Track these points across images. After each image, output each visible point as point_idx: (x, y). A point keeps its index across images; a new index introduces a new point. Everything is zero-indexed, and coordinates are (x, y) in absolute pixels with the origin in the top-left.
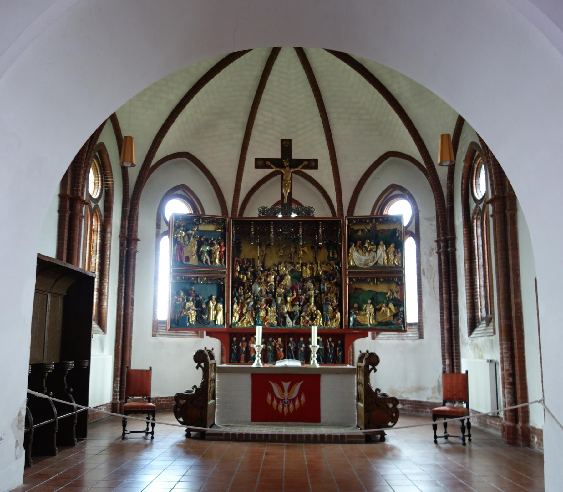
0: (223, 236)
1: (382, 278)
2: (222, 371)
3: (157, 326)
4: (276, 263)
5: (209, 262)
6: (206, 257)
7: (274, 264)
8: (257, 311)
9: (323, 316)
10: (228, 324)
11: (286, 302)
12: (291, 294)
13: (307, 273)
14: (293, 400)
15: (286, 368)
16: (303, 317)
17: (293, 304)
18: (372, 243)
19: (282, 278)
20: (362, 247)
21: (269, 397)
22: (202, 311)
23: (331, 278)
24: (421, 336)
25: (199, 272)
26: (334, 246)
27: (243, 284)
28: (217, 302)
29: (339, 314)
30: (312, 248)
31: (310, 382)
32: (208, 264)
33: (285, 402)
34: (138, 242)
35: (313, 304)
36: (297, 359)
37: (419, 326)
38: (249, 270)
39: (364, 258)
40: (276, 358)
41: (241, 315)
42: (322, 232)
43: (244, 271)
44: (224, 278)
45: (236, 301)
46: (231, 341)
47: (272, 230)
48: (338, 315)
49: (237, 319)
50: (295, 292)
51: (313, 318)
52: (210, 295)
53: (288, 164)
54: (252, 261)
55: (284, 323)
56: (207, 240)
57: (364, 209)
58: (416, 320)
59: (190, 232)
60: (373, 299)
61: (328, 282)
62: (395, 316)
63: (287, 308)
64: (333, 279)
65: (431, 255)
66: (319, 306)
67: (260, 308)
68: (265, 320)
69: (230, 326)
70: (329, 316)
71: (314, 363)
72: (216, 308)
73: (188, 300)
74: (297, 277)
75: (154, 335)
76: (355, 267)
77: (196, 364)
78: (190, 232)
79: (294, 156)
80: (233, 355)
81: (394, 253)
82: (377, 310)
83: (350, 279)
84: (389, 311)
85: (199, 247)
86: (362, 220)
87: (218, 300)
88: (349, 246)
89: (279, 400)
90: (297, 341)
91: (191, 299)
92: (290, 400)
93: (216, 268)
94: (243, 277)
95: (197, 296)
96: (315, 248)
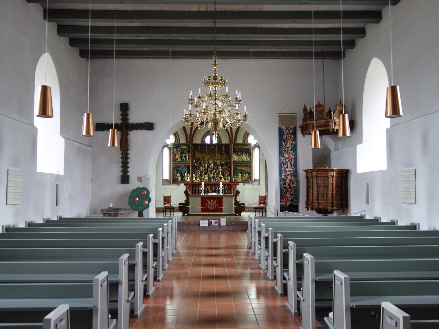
0: (189, 150)
2: (191, 196)
3: (164, 180)
6: (183, 158)
8: (201, 176)
9: (224, 178)
11: (211, 173)
13: (219, 163)
14: (214, 205)
15: (212, 195)
17: (214, 174)
19: (210, 165)
20: (237, 154)
21: (207, 205)
22: (183, 177)
24: (259, 184)
26: (228, 153)
27: (196, 167)
30: (220, 154)
31: (219, 200)
36: (215, 192)
37: (259, 180)
39: (238, 158)
40: (208, 193)
41: (196, 178)
43: (196, 162)
46: (193, 187)
51: (221, 179)
55: (211, 181)
56: (184, 152)
57: (240, 141)
58: (258, 179)
60: (241, 172)
62: (248, 178)
63: (212, 175)
66: (223, 175)
68: (204, 179)
69: (192, 182)
70: (226, 178)
71: (221, 194)
72: (187, 176)
74: (215, 164)
75: (163, 185)
76: (235, 161)
82: (242, 176)
83: (234, 165)
84: (246, 176)
85: (181, 154)
86: (238, 145)
87: (188, 173)
88: (233, 154)
90: (215, 187)
95: (181, 172)
96: (221, 153)
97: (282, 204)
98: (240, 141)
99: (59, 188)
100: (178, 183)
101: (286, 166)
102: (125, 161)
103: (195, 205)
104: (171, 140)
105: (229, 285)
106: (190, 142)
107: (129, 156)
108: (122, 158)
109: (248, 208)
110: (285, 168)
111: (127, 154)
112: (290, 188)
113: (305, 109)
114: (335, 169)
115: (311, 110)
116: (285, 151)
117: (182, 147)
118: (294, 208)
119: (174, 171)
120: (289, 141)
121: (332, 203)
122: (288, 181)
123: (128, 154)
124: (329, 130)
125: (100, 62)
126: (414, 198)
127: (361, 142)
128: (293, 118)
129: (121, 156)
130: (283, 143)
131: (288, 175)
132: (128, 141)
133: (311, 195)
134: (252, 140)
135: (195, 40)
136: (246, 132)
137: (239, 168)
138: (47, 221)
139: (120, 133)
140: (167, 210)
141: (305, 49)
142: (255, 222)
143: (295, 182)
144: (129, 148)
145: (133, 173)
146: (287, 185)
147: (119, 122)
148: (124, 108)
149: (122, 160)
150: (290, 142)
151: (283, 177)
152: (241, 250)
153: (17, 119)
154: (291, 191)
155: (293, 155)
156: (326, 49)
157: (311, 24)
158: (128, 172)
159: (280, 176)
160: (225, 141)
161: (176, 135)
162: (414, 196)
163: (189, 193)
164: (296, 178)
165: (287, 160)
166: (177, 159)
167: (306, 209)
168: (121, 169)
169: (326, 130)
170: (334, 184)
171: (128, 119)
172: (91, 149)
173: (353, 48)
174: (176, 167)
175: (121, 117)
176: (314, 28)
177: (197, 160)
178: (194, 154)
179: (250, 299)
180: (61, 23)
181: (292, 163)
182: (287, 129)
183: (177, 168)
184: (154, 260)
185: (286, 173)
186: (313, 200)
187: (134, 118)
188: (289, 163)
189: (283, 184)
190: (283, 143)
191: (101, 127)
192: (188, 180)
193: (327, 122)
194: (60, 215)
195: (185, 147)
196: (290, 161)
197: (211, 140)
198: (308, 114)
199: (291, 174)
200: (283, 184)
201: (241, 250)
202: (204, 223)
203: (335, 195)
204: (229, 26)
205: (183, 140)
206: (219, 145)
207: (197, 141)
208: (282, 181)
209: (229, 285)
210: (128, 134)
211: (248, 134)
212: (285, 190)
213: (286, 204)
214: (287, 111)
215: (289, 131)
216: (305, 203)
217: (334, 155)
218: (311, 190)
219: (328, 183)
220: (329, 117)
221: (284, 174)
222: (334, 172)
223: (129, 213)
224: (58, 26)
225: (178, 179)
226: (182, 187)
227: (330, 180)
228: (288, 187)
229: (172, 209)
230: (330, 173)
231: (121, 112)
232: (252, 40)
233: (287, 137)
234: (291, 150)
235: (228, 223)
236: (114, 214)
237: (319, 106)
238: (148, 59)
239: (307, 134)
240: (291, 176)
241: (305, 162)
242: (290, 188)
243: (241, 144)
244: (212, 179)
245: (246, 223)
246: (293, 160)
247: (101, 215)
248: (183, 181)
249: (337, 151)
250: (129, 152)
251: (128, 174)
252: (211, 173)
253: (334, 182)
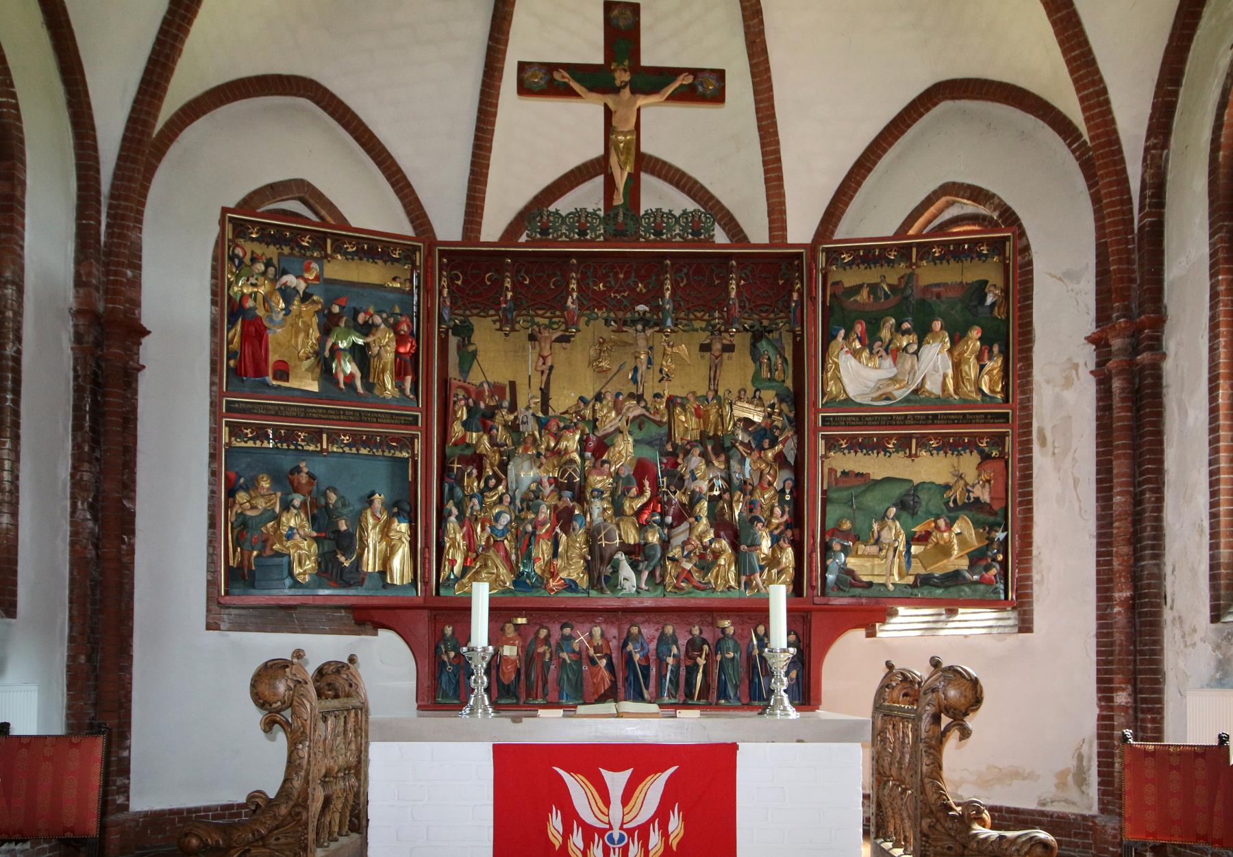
1: (936, 436)
4: (589, 396)
5: (358, 383)
7: (581, 399)
8: (526, 542)
10: (426, 583)
12: (634, 491)
16: (673, 559)
18: (906, 325)
21: (556, 823)
22: (337, 544)
23: (766, 443)
24: (1025, 626)
25: (326, 416)
28: (392, 516)
29: (790, 552)
32: (355, 389)
33: (611, 838)
34: (145, 341)
35: (704, 521)
38: (498, 418)
42: (739, 294)
44: (414, 437)
45: (455, 511)
47: (573, 286)
48: (788, 556)
49: (457, 569)
50: (647, 483)
52: (368, 492)
53: (626, 77)
55: (612, 582)
59: (290, 280)
60: (902, 505)
61: (756, 454)
64: (772, 446)
65: (1068, 383)
67: (533, 533)
73: (287, 506)
77: (945, 664)
78: (290, 280)
79: (646, 60)
80: (444, 679)
81: (979, 358)
85: (327, 329)
88: (829, 338)
89: (589, 833)
91: (297, 502)
92: (630, 832)
93: (385, 403)
94: (479, 439)
117: (340, 269)
192: (400, 564)
238: (412, 179)
244: (626, 571)
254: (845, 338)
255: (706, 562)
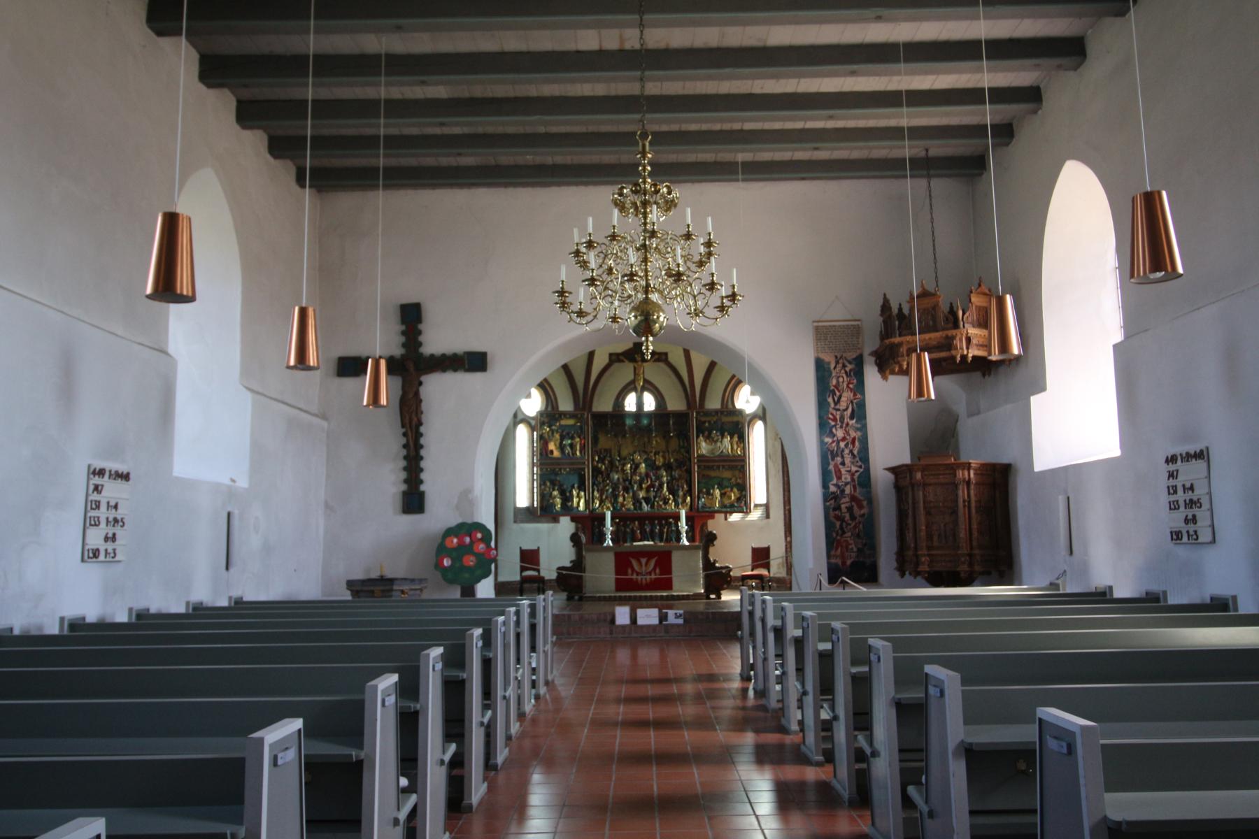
3: (518, 511)
8: (615, 497)
9: (675, 500)
13: (660, 461)
14: (650, 573)
20: (708, 438)
22: (566, 499)
24: (768, 516)
41: (601, 502)
43: (602, 460)
54: (608, 451)
55: (641, 508)
57: (713, 403)
62: (738, 499)
63: (641, 494)
66: (671, 491)
72: (578, 496)
74: (651, 465)
82: (722, 495)
85: (562, 438)
96: (666, 436)
97: (833, 561)
98: (713, 403)
99: (236, 522)
100: (555, 519)
101: (839, 459)
102: (413, 453)
103: (602, 572)
104: (533, 404)
105: (697, 777)
106: (584, 409)
107: (422, 441)
108: (405, 446)
109: (736, 579)
110: (836, 466)
111: (418, 435)
112: (853, 518)
113: (886, 307)
114: (974, 462)
115: (900, 309)
116: (835, 419)
117: (564, 422)
118: (867, 573)
119: (545, 484)
120: (845, 394)
121: (970, 555)
122: (847, 499)
123: (421, 435)
124: (954, 358)
125: (346, 201)
126: (1210, 530)
127: (1040, 387)
128: (854, 331)
129: (404, 441)
130: (830, 400)
131: (847, 484)
132: (421, 401)
133: (909, 535)
134: (746, 401)
135: (593, 133)
136: (733, 376)
137: (713, 474)
138: (195, 609)
139: (398, 381)
140: (526, 586)
141: (880, 150)
142: (764, 602)
143: (865, 503)
144: (424, 420)
145: (431, 484)
146: (844, 510)
147: (398, 351)
148: (411, 316)
149: (404, 452)
150: (847, 396)
151: (832, 489)
152: (725, 685)
153: (119, 333)
154: (855, 527)
155: (857, 429)
156: (939, 148)
157: (896, 78)
158: (421, 482)
159: (825, 485)
160: (676, 404)
161: (544, 387)
162: (1209, 523)
163: (584, 539)
164: (869, 492)
165: (842, 445)
166: (552, 452)
167: (897, 573)
168: (403, 475)
169: (945, 359)
170: (973, 504)
171: (420, 344)
172: (325, 424)
173: (1007, 145)
174: (549, 472)
175: (403, 339)
176: (907, 91)
177: (604, 455)
178: (595, 441)
179: (757, 817)
180: (246, 94)
181: (855, 452)
182: (837, 363)
183: (553, 477)
184: (486, 707)
185: (839, 478)
186: (916, 549)
187: (435, 341)
188: (847, 451)
189: (835, 509)
190: (830, 400)
191: (350, 367)
192: (582, 507)
193: (947, 337)
194: (236, 593)
195: (571, 422)
196: (850, 446)
197: (640, 404)
198: (894, 321)
199: (853, 480)
200: (835, 509)
201: (725, 685)
202: (622, 615)
203: (975, 534)
204: (681, 92)
205: (566, 405)
206: (661, 414)
207: (603, 405)
208: (831, 500)
209: (697, 777)
210: (421, 383)
211: (739, 382)
212: (838, 524)
213: (844, 563)
214: (837, 314)
215: (844, 366)
216: (894, 557)
217: (967, 428)
218: (910, 521)
219: (957, 501)
220: (951, 325)
221: (835, 481)
222: (972, 472)
223: (421, 590)
224: (239, 102)
225: (554, 505)
226: (566, 526)
227: (960, 493)
228: (847, 516)
229: (539, 585)
230: (960, 474)
231: (403, 328)
232: (742, 131)
233: (841, 371)
234: (852, 418)
235: (690, 618)
236: (383, 591)
237: (924, 294)
239: (893, 373)
240: (854, 487)
241: (889, 444)
242: (853, 518)
243: (717, 412)
245: (737, 616)
246: (857, 443)
247: (347, 596)
248: (567, 509)
249: (975, 419)
250: (422, 429)
251: (422, 488)
252: (641, 488)
253: (973, 498)
254: (692, 440)
255: (666, 502)
